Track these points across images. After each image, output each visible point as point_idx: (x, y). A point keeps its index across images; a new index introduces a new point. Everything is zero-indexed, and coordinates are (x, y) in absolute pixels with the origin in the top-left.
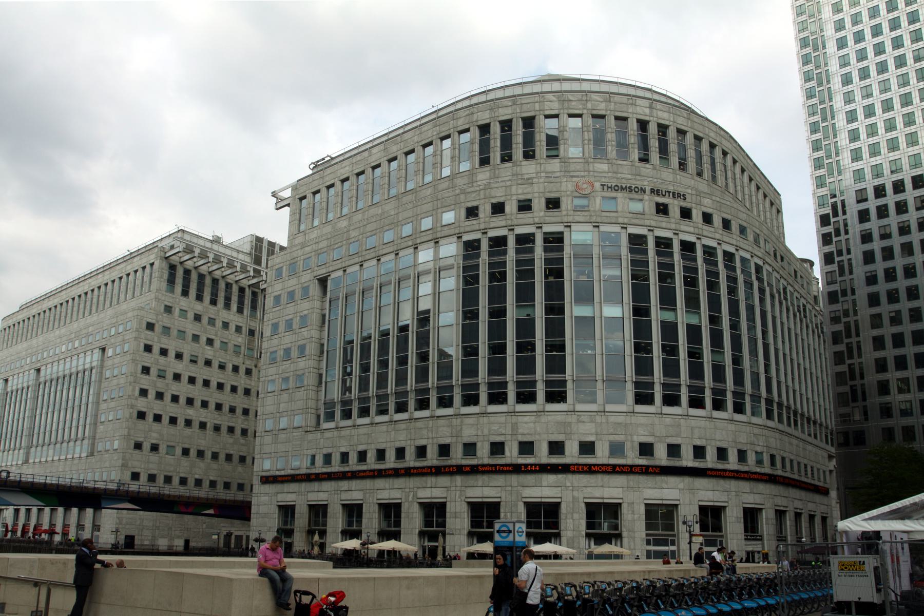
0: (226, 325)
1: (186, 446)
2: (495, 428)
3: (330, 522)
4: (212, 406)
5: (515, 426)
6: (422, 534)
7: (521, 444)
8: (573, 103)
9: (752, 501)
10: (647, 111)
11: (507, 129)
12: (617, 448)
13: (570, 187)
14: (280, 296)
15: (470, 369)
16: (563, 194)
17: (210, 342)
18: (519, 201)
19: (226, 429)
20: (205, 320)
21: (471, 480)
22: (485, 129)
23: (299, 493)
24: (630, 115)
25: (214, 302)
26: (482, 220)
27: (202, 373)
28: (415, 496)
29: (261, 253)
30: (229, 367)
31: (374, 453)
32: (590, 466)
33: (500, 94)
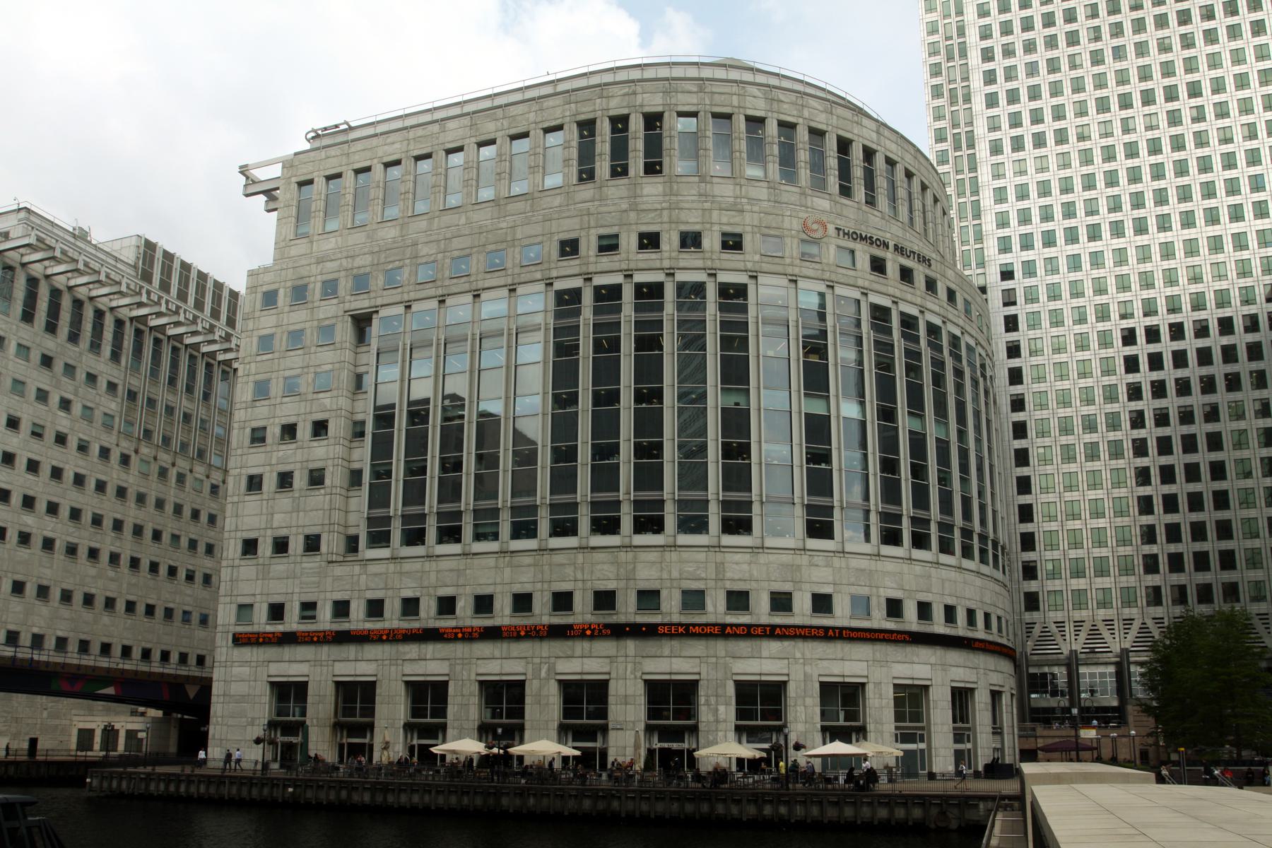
0: (91, 378)
1: (19, 578)
2: (690, 568)
3: (381, 710)
4: (64, 512)
5: (720, 567)
6: (408, 727)
7: (730, 594)
8: (785, 106)
9: (579, 670)
10: (874, 136)
11: (620, 130)
12: (862, 604)
13: (796, 224)
14: (272, 336)
15: (563, 480)
16: (786, 232)
17: (65, 404)
18: (601, 237)
19: (86, 552)
20: (58, 366)
21: (651, 646)
22: (587, 127)
23: (316, 662)
24: (855, 138)
25: (74, 338)
26: (666, 255)
27: (49, 455)
28: (551, 669)
29: (152, 266)
30: (95, 449)
31: (471, 601)
32: (826, 629)
33: (608, 78)
